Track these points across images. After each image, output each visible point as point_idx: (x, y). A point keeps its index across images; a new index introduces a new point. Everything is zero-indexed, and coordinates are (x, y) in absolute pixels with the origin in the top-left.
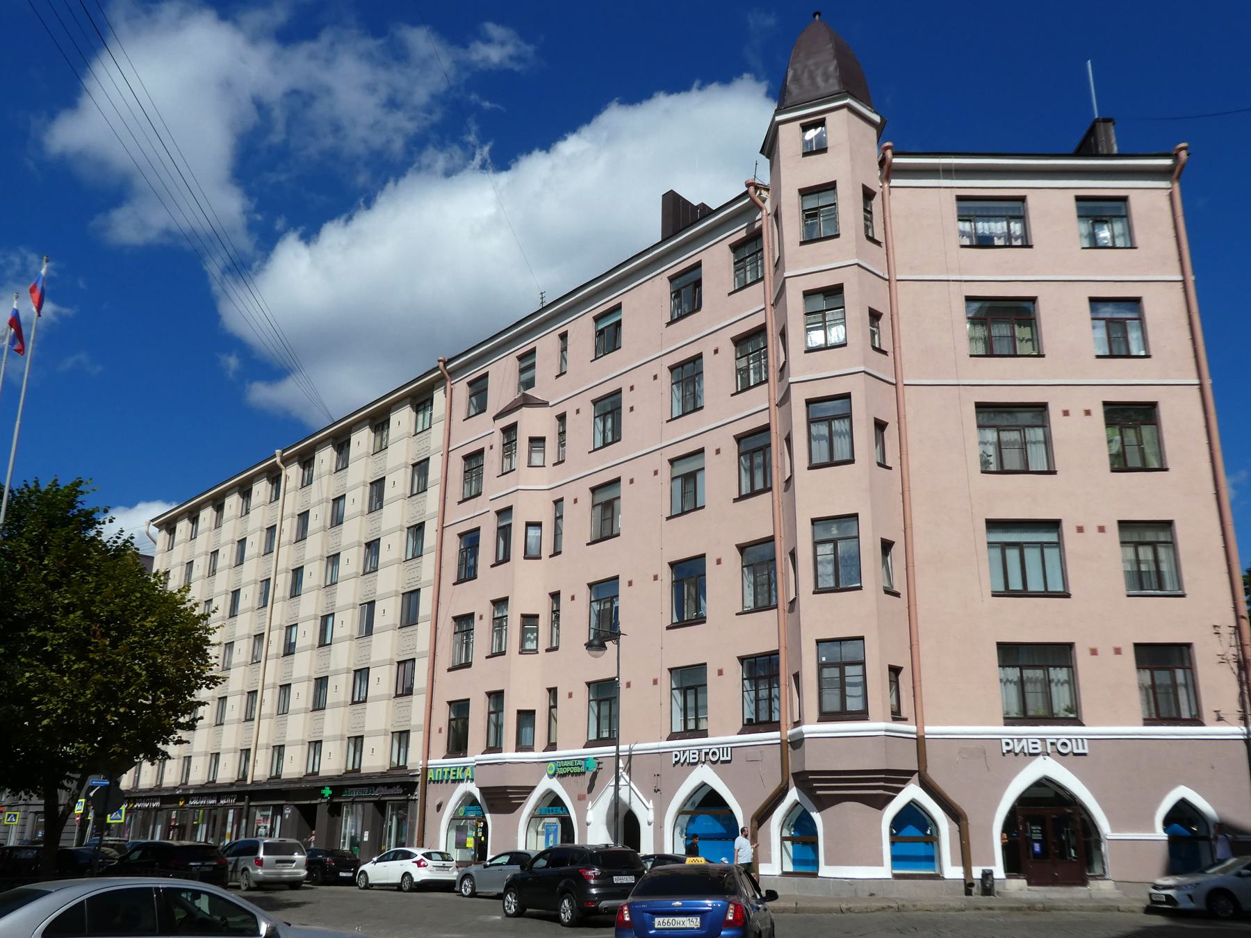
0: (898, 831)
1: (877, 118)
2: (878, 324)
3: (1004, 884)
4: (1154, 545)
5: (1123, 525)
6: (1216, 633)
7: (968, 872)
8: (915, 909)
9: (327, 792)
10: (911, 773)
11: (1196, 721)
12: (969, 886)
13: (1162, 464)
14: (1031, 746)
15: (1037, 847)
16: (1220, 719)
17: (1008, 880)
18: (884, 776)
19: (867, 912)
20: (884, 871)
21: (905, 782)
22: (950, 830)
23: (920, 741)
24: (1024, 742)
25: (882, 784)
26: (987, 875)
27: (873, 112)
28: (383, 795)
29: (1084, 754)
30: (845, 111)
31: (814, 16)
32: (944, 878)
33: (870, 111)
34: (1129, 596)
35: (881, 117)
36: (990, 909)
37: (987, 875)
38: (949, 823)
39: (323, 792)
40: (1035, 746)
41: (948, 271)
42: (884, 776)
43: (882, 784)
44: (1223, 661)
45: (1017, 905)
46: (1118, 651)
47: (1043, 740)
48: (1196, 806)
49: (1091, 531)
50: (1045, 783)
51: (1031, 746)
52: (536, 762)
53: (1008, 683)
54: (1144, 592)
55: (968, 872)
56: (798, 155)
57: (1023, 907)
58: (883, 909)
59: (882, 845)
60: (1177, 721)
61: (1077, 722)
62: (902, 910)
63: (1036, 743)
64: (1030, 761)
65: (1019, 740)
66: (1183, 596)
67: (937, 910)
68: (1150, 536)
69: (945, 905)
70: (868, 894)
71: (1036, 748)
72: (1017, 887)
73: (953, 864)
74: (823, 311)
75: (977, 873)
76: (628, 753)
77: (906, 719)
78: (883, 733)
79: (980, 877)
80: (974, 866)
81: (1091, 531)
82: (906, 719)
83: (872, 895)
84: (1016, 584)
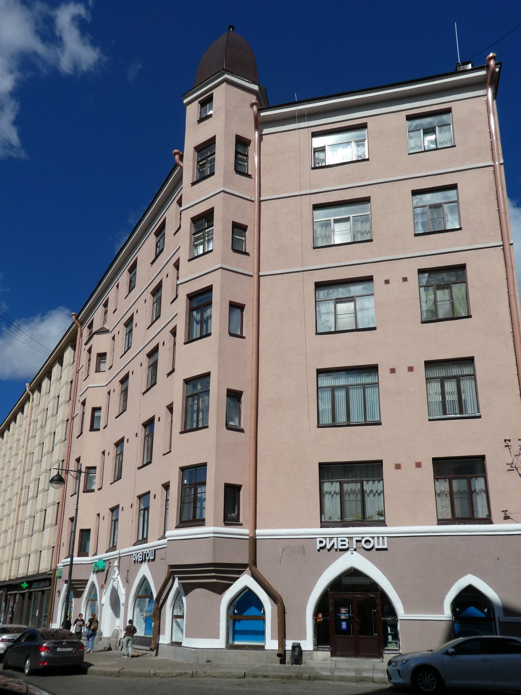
0: (461, 611)
1: (256, 87)
2: (245, 235)
3: (312, 655)
4: (458, 379)
5: (429, 364)
6: (506, 446)
7: (282, 644)
8: (205, 675)
9: (25, 585)
10: (245, 566)
11: (488, 520)
12: (282, 656)
13: (468, 313)
14: (340, 543)
15: (344, 625)
16: (507, 518)
17: (315, 652)
18: (213, 568)
19: (169, 677)
20: (220, 643)
21: (240, 573)
22: (272, 610)
23: (253, 541)
24: (335, 540)
25: (214, 574)
26: (296, 647)
27: (251, 83)
28: (44, 587)
29: (386, 549)
30: (224, 84)
31: (229, 29)
32: (265, 650)
33: (248, 82)
34: (430, 420)
35: (259, 86)
36: (265, 676)
37: (296, 647)
38: (272, 605)
39: (22, 585)
40: (343, 543)
41: (301, 188)
42: (213, 568)
43: (214, 574)
44: (512, 469)
45: (287, 674)
46: (418, 465)
47: (351, 538)
48: (482, 592)
49: (402, 371)
50: (353, 573)
51: (340, 543)
52: (89, 564)
53: (335, 495)
54: (446, 416)
55: (282, 644)
56: (195, 124)
57: (292, 676)
58: (181, 675)
59: (219, 622)
60: (472, 519)
61: (383, 523)
62: (195, 676)
63: (345, 541)
64: (340, 556)
65: (331, 539)
66: (479, 417)
67: (222, 677)
68: (455, 371)
69: (228, 673)
70: (205, 660)
71: (345, 545)
72: (324, 655)
73: (272, 638)
74: (202, 230)
75: (289, 646)
76: (118, 556)
77: (241, 525)
78: (212, 535)
79: (291, 649)
80: (289, 640)
81: (402, 371)
82: (241, 525)
83: (208, 661)
84: (342, 418)
